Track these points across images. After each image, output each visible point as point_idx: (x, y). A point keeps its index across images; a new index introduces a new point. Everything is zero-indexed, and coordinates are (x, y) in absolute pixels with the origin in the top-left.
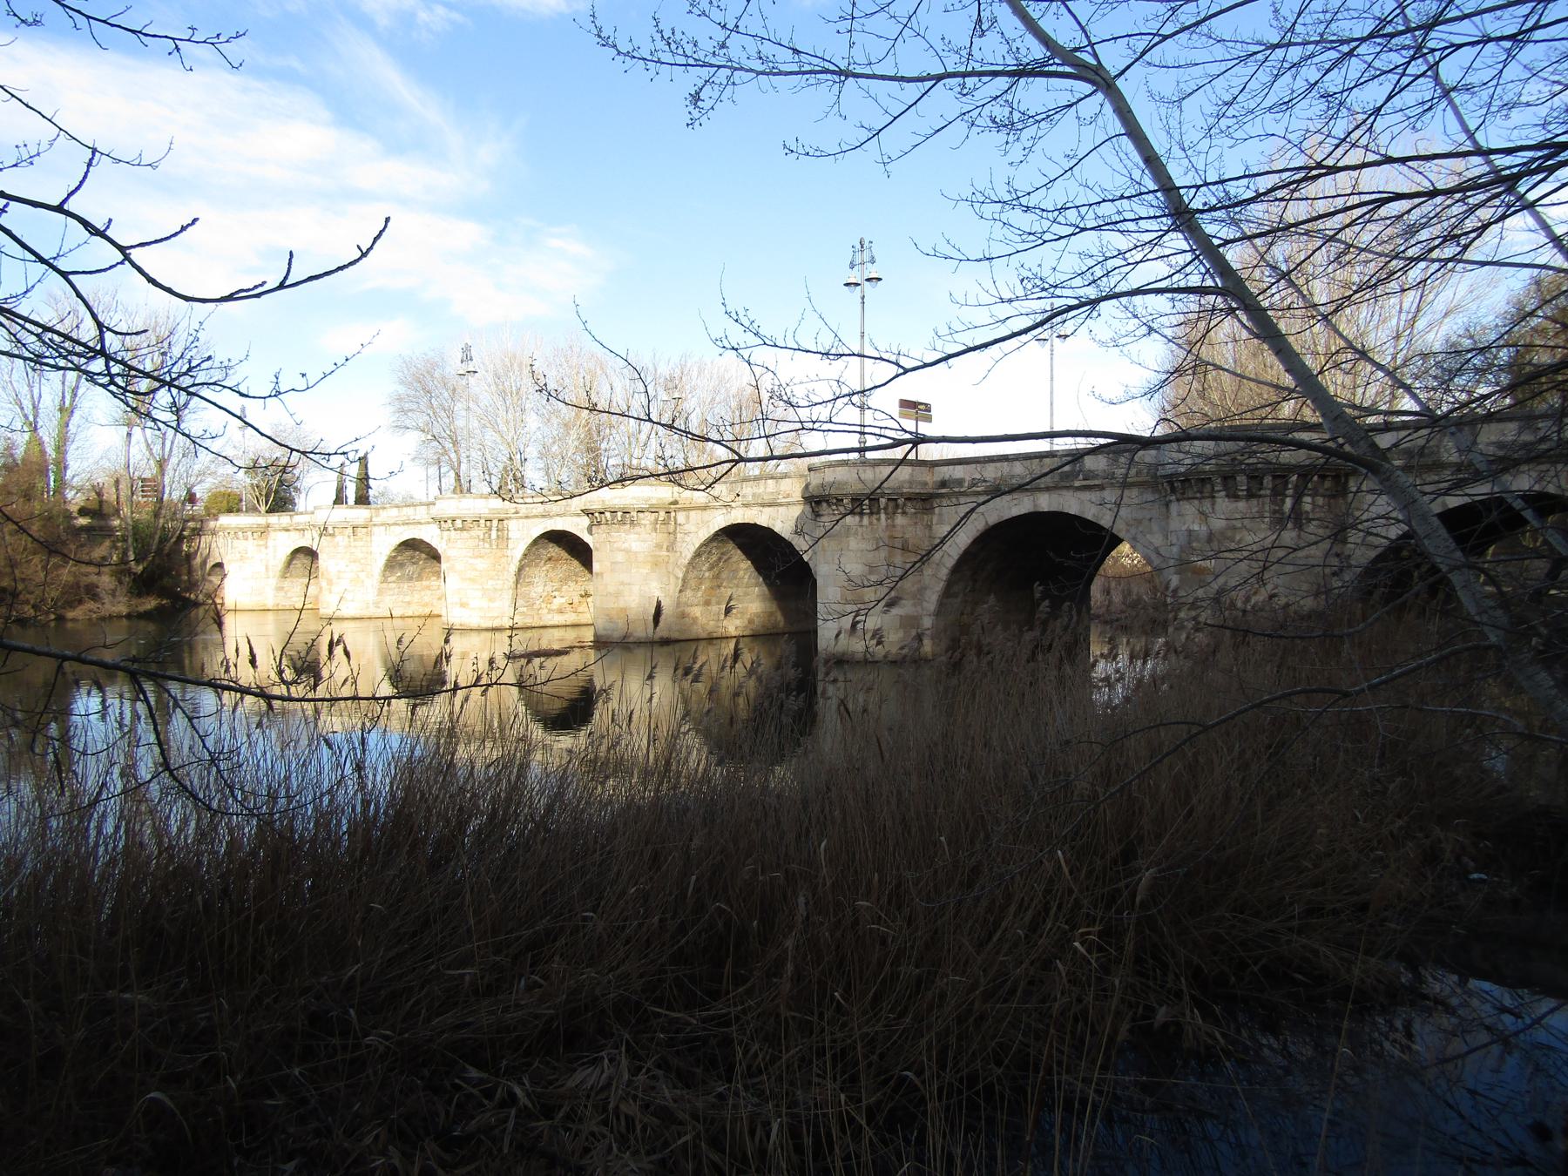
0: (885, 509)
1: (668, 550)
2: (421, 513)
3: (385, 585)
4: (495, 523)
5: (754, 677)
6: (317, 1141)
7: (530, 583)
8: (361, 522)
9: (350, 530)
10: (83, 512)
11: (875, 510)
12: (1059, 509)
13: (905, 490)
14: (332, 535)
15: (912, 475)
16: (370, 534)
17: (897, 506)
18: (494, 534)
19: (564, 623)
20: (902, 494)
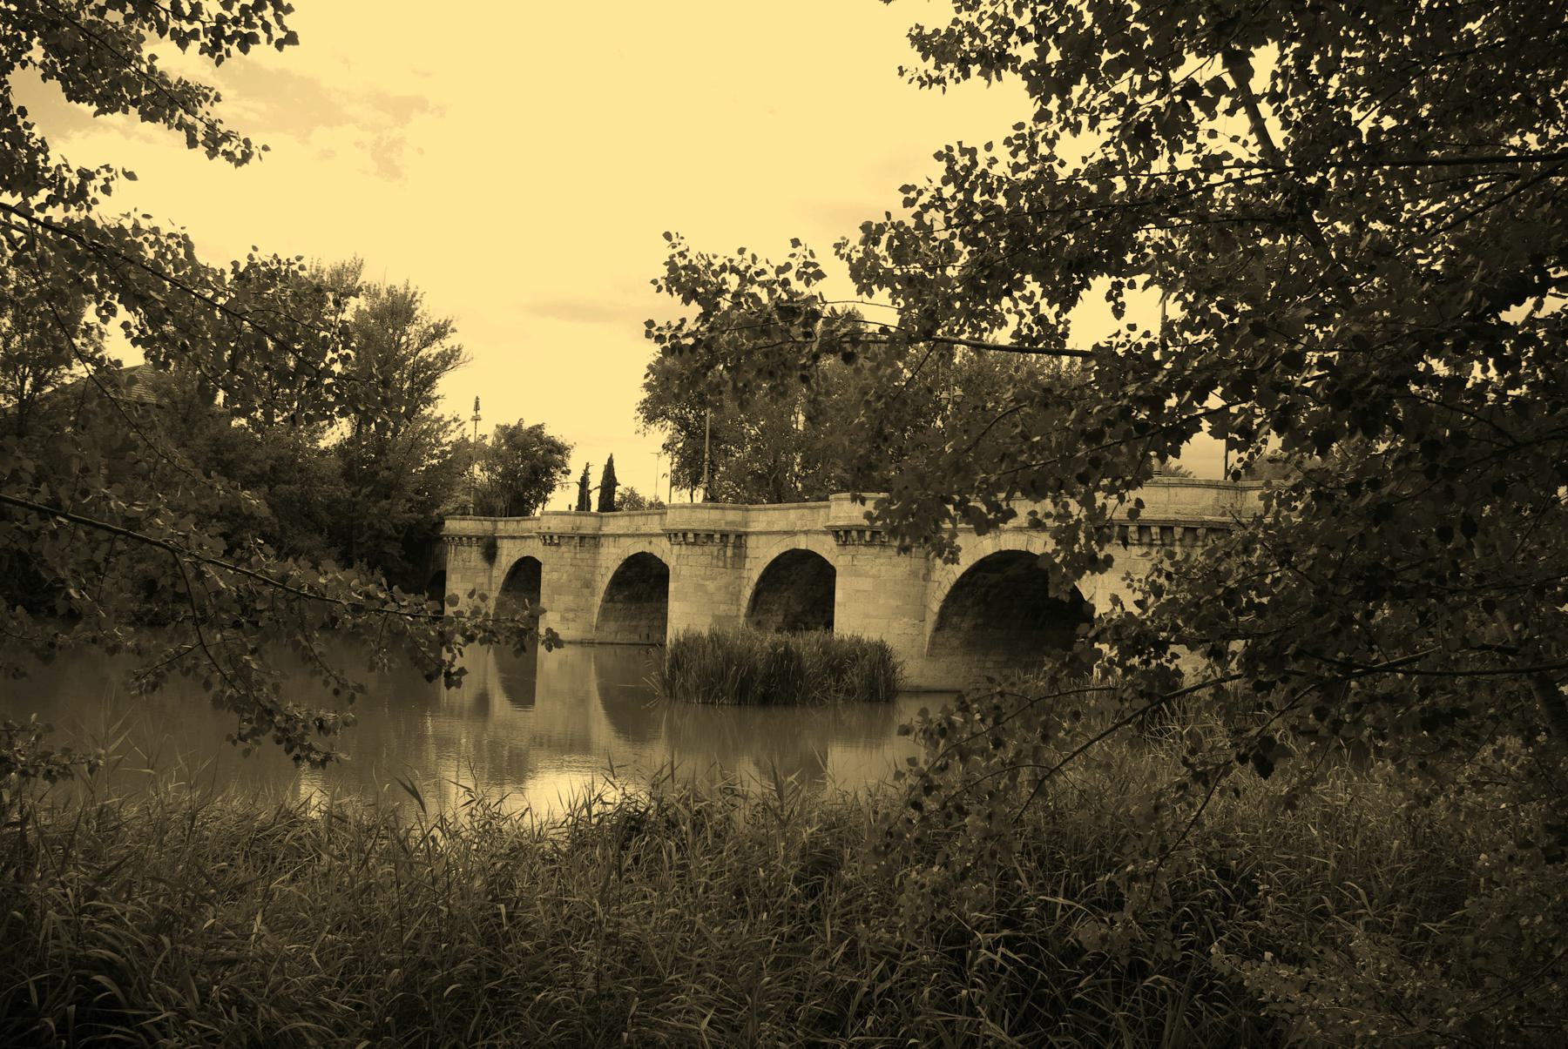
0: (1180, 540)
1: (924, 579)
2: (653, 524)
3: (610, 605)
4: (732, 539)
5: (254, 541)
6: (373, 426)
7: (768, 611)
8: (588, 531)
9: (577, 540)
10: (86, 324)
11: (1167, 541)
12: (978, 558)
13: (1206, 518)
14: (558, 545)
15: (1217, 500)
16: (597, 546)
17: (1196, 538)
18: (729, 552)
19: (949, 687)
20: (1203, 523)
